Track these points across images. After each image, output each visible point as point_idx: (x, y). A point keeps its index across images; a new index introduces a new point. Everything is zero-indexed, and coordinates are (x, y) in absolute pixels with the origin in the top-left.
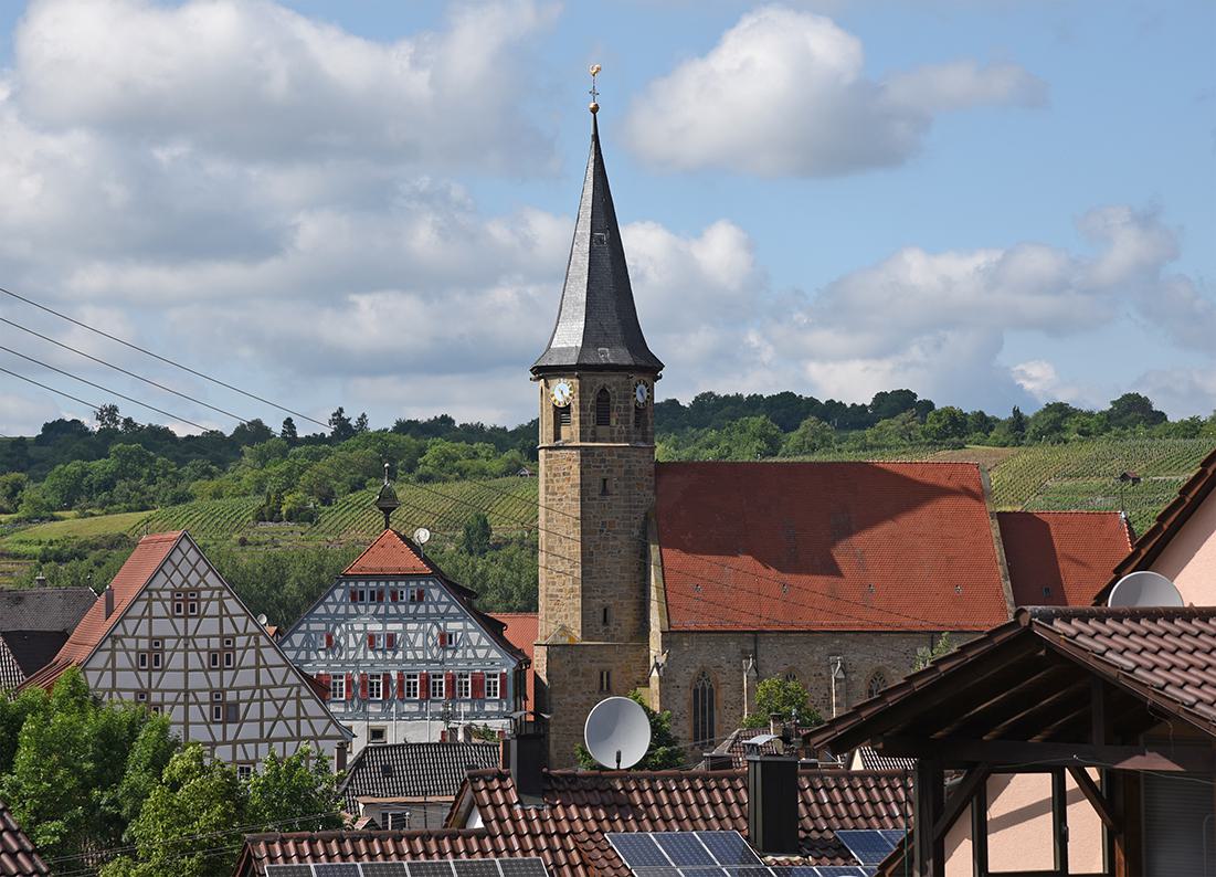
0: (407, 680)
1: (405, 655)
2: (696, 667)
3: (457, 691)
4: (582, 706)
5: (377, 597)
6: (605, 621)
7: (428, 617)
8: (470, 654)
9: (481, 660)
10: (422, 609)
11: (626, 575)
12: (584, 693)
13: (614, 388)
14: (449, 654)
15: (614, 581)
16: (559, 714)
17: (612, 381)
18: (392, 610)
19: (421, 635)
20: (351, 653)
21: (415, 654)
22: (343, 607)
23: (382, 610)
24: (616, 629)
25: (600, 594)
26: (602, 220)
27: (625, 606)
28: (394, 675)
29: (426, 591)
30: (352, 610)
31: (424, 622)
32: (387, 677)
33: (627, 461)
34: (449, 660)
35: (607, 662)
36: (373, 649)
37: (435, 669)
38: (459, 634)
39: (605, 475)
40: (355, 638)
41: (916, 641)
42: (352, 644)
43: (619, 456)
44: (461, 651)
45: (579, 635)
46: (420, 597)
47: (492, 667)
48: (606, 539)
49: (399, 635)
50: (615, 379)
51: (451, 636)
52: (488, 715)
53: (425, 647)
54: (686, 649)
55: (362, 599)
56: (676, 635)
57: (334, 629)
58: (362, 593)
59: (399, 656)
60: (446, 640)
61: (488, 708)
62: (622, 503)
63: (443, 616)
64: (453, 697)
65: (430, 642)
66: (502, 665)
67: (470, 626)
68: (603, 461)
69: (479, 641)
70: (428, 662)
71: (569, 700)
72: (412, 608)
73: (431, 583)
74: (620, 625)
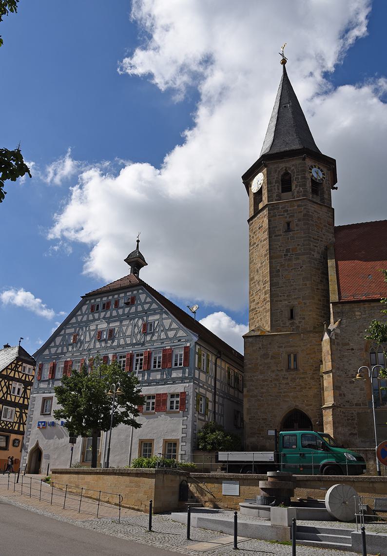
0: (119, 360)
1: (119, 342)
5: (106, 307)
6: (292, 317)
7: (137, 315)
8: (163, 336)
9: (171, 339)
10: (133, 309)
11: (308, 282)
12: (273, 371)
13: (293, 168)
14: (148, 338)
15: (297, 287)
16: (252, 387)
17: (292, 165)
18: (114, 313)
19: (130, 327)
20: (86, 345)
21: (125, 341)
22: (86, 316)
23: (108, 315)
24: (300, 322)
25: (286, 298)
26: (286, 100)
27: (308, 304)
28: (110, 356)
29: (137, 298)
30: (91, 317)
31: (134, 319)
32: (106, 358)
33: (305, 209)
34: (148, 342)
35: (291, 347)
36: (100, 340)
37: (138, 349)
38: (156, 322)
39: (288, 219)
40: (90, 334)
42: (88, 339)
43: (298, 206)
44: (157, 334)
45: (269, 329)
46: (130, 303)
47: (179, 343)
49: (116, 329)
50: (294, 163)
51: (151, 325)
52: (174, 381)
53: (133, 335)
54: (358, 317)
55: (97, 309)
56: (347, 307)
57: (79, 330)
58: (98, 306)
59: (115, 343)
60: (147, 329)
61: (174, 375)
63: (146, 313)
64: (149, 369)
65: (136, 331)
66: (187, 341)
67: (164, 316)
69: (171, 325)
70: (133, 345)
71: (261, 377)
72: (127, 310)
73: (140, 291)
74: (304, 318)
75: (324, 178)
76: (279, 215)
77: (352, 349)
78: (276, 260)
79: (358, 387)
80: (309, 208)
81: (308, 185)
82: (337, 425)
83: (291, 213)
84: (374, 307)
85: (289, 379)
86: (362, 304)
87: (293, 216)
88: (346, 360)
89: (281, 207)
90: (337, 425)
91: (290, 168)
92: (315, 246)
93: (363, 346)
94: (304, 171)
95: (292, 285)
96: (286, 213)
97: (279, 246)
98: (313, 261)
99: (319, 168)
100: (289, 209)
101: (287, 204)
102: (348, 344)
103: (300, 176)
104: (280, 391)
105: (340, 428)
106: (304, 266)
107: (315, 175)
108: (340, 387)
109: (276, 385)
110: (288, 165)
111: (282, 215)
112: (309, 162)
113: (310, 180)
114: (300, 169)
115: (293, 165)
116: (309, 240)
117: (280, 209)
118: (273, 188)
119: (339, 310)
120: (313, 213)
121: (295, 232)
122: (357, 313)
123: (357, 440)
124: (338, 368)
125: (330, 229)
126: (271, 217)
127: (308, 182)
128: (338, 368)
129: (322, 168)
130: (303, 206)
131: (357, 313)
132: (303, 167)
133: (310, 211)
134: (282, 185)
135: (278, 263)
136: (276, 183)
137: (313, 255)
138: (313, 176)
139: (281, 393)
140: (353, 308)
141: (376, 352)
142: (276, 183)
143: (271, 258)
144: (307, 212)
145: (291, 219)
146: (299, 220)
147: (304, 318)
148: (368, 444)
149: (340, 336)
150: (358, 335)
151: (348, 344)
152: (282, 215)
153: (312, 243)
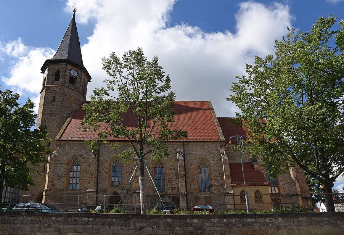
2: (71, 155)
3: (199, 213)
4: (34, 177)
13: (61, 69)
17: (61, 67)
39: (54, 95)
41: (176, 146)
43: (60, 89)
48: (51, 116)
54: (67, 148)
56: (63, 142)
62: (59, 104)
68: (54, 91)
74: (54, 146)
75: (78, 76)
76: (50, 93)
77: (62, 163)
78: (45, 115)
79: (62, 181)
80: (65, 90)
81: (66, 79)
82: (47, 199)
83: (56, 92)
84: (74, 143)
85: (43, 176)
86: (69, 141)
87: (56, 94)
88: (58, 168)
89: (52, 88)
90: (47, 199)
91: (59, 69)
92: (65, 110)
93: (67, 162)
94: (66, 71)
95: (51, 129)
96: (53, 92)
97: (48, 109)
98: (63, 118)
99: (75, 70)
100: (55, 90)
101: (55, 87)
102: (60, 161)
103: (63, 74)
104: (38, 182)
105: (50, 201)
106: (58, 120)
107: (72, 74)
108: (53, 181)
109: (36, 179)
110: (59, 67)
111: (52, 93)
112: (70, 67)
113: (69, 76)
114: (64, 70)
115: (61, 67)
116: (62, 107)
117: (51, 89)
118: (50, 78)
119: (59, 144)
120: (67, 94)
121: (56, 102)
122: (67, 146)
123: (58, 207)
124: (53, 172)
125: (77, 102)
126: (47, 93)
127: (67, 77)
128: (53, 172)
129: (77, 70)
130: (62, 89)
131: (67, 146)
132: (66, 69)
133: (65, 92)
134: (56, 77)
135: (46, 117)
136: (51, 76)
137: (63, 115)
138: (71, 74)
139: (38, 183)
140: (65, 143)
141: (74, 165)
142: (51, 76)
143: (43, 114)
144: (63, 92)
145: (55, 95)
146: (59, 96)
147: (54, 146)
148: (62, 209)
149: (57, 157)
150: (66, 156)
151: (60, 161)
152: (52, 93)
153: (63, 109)
